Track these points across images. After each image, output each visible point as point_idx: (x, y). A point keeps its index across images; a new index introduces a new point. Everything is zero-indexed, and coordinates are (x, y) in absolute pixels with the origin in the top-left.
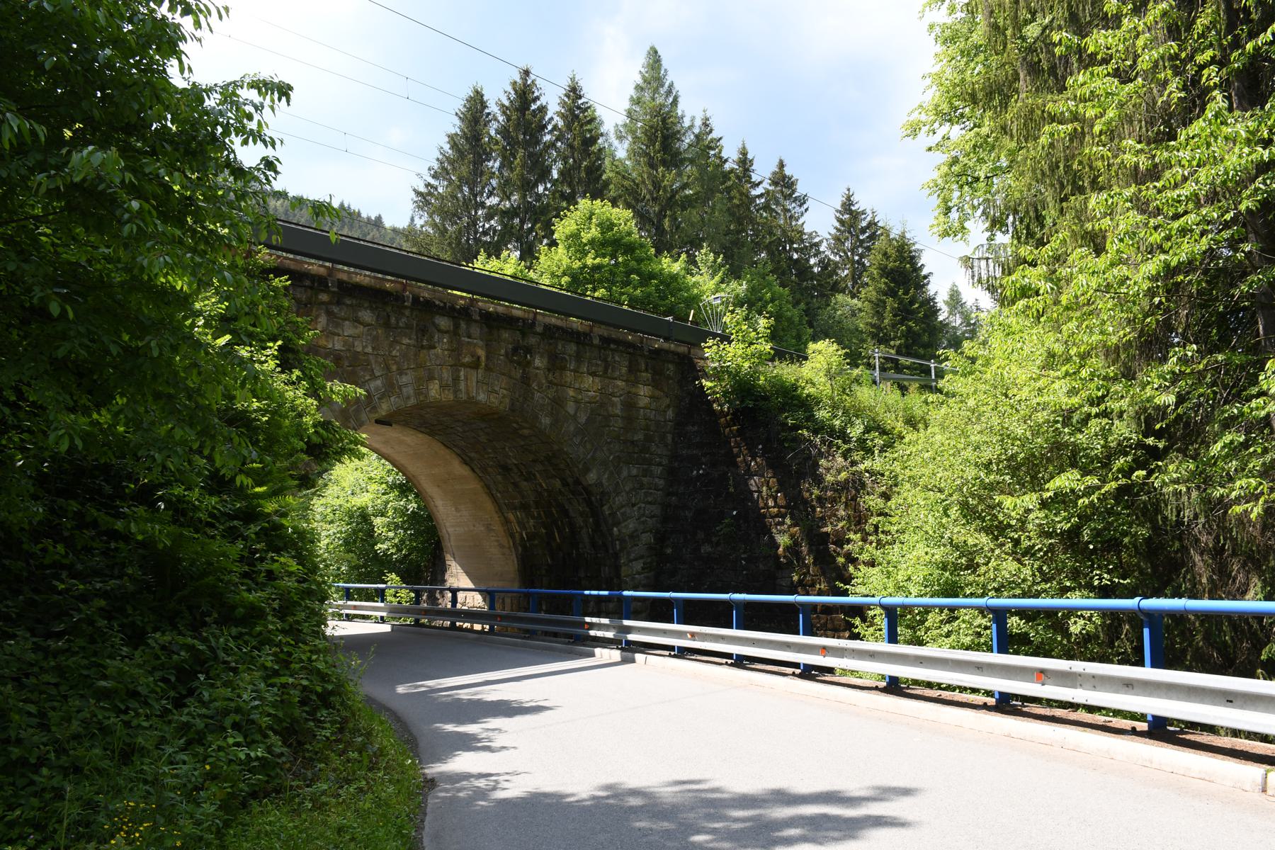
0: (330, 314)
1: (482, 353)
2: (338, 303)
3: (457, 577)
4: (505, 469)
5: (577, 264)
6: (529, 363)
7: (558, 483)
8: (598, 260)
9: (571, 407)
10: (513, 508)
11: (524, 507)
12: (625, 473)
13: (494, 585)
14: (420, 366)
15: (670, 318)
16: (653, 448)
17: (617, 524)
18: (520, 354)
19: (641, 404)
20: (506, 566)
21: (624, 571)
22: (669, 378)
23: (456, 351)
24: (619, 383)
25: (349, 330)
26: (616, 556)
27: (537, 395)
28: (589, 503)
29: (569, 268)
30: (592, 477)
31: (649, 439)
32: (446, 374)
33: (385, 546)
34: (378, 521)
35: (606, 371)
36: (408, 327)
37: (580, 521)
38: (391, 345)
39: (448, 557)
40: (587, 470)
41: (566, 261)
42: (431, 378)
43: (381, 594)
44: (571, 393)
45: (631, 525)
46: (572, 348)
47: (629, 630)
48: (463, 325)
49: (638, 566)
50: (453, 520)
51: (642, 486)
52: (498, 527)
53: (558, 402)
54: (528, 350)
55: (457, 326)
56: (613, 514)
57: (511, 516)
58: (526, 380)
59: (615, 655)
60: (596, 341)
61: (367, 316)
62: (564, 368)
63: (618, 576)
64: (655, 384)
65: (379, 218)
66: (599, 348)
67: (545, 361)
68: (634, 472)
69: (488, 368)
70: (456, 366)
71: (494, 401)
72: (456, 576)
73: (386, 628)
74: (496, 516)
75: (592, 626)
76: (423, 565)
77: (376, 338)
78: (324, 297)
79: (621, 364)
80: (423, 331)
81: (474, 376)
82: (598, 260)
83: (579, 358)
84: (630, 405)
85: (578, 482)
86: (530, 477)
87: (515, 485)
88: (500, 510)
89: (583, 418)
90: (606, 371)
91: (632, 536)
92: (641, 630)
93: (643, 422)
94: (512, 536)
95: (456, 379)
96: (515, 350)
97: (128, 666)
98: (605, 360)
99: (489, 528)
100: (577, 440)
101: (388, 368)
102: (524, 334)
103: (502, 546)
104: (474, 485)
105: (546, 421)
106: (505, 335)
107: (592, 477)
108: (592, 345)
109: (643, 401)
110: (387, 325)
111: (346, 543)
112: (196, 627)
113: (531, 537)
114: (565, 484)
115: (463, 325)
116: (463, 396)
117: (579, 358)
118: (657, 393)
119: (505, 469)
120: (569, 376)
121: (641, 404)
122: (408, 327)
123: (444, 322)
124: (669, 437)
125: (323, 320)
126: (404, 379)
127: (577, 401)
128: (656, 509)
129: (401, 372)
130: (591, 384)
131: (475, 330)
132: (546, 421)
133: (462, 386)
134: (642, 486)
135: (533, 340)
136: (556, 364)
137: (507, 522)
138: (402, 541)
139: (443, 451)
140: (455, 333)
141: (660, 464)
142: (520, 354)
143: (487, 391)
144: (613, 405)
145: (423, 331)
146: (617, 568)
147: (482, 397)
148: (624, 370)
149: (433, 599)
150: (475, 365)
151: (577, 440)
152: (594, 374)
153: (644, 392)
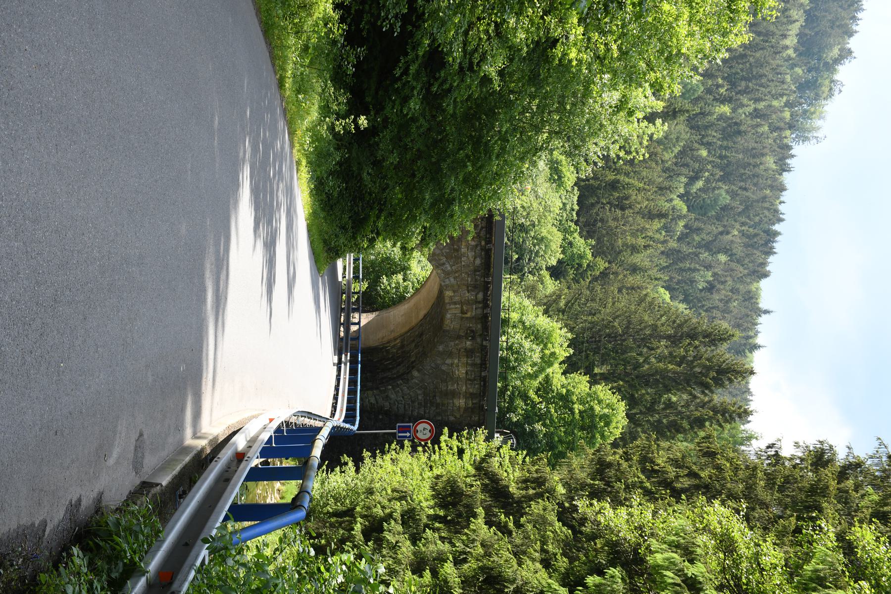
0: (476, 246)
1: (469, 315)
2: (482, 249)
3: (366, 319)
4: (421, 335)
5: (575, 398)
6: (467, 338)
7: (413, 359)
8: (577, 411)
9: (449, 361)
10: (402, 342)
11: (402, 346)
12: (419, 392)
13: (362, 336)
14: (459, 286)
15: (497, 411)
16: (433, 408)
17: (393, 388)
18: (471, 334)
19: (455, 401)
20: (373, 341)
21: (370, 392)
22: (471, 417)
23: (468, 302)
24: (464, 388)
25: (471, 254)
26: (377, 388)
27: (452, 343)
28: (403, 374)
29: (573, 393)
30: (415, 373)
31: (438, 405)
32: (457, 299)
33: (385, 281)
34: (400, 277)
35: (470, 380)
36: (476, 280)
37: (395, 371)
38: (466, 273)
39: (377, 313)
40: (419, 371)
41: (577, 391)
42: (454, 292)
43: (356, 277)
44: (456, 361)
45: (393, 396)
46: (478, 361)
47: (345, 364)
48: (480, 305)
49: (373, 400)
50: (397, 315)
51: (413, 402)
52: (392, 336)
53: (450, 355)
54: (473, 338)
55: (479, 302)
56: (398, 386)
57: (398, 341)
58: (459, 337)
59: (336, 361)
60: (483, 374)
61: (478, 262)
62: (468, 357)
63: (368, 390)
64: (466, 409)
65: (766, 275)
66: (480, 376)
67: (470, 347)
68: (420, 398)
69: (462, 318)
70: (461, 303)
71: (447, 322)
72: (367, 317)
73: (340, 279)
74: (398, 334)
75: (346, 355)
76: (370, 301)
77: (469, 266)
78: (483, 243)
79: (474, 389)
80: (475, 287)
81: (458, 312)
82: (577, 411)
83: (473, 365)
84: (454, 394)
85: (413, 367)
86: (416, 346)
87: (414, 341)
88: (401, 336)
89: (444, 368)
90: (470, 380)
91: (387, 396)
92: (346, 370)
93: (446, 402)
94: (388, 342)
95: (455, 303)
96: (472, 331)
97: (346, 217)
98: (475, 380)
99: (393, 331)
100: (433, 365)
101: (456, 272)
102: (480, 335)
103: (383, 338)
104: (414, 322)
105: (441, 348)
106: (479, 326)
107: (415, 373)
108: (481, 371)
109: (457, 402)
110: (475, 271)
111: (388, 258)
112: (352, 228)
113: (388, 351)
114: (413, 362)
115: (480, 305)
116: (448, 307)
117: (473, 365)
118: (462, 410)
119: (421, 335)
120: (464, 360)
121: (455, 401)
122: (476, 280)
123: (480, 296)
124: (440, 418)
125: (473, 243)
126: (452, 280)
127: (452, 364)
128: (402, 411)
129: (455, 278)
130: (461, 372)
131: (479, 311)
132: (441, 348)
133: (452, 306)
134: (413, 402)
135: (479, 340)
136: (469, 353)
137: (395, 339)
138: (388, 292)
139: (431, 304)
140: (477, 302)
141: (425, 412)
142: (471, 334)
143: (451, 318)
144: (453, 385)
145: (475, 287)
146: (371, 389)
147: (448, 316)
148: (471, 390)
149: (354, 310)
150: (463, 312)
151: (433, 365)
152: (467, 373)
153: (461, 402)
